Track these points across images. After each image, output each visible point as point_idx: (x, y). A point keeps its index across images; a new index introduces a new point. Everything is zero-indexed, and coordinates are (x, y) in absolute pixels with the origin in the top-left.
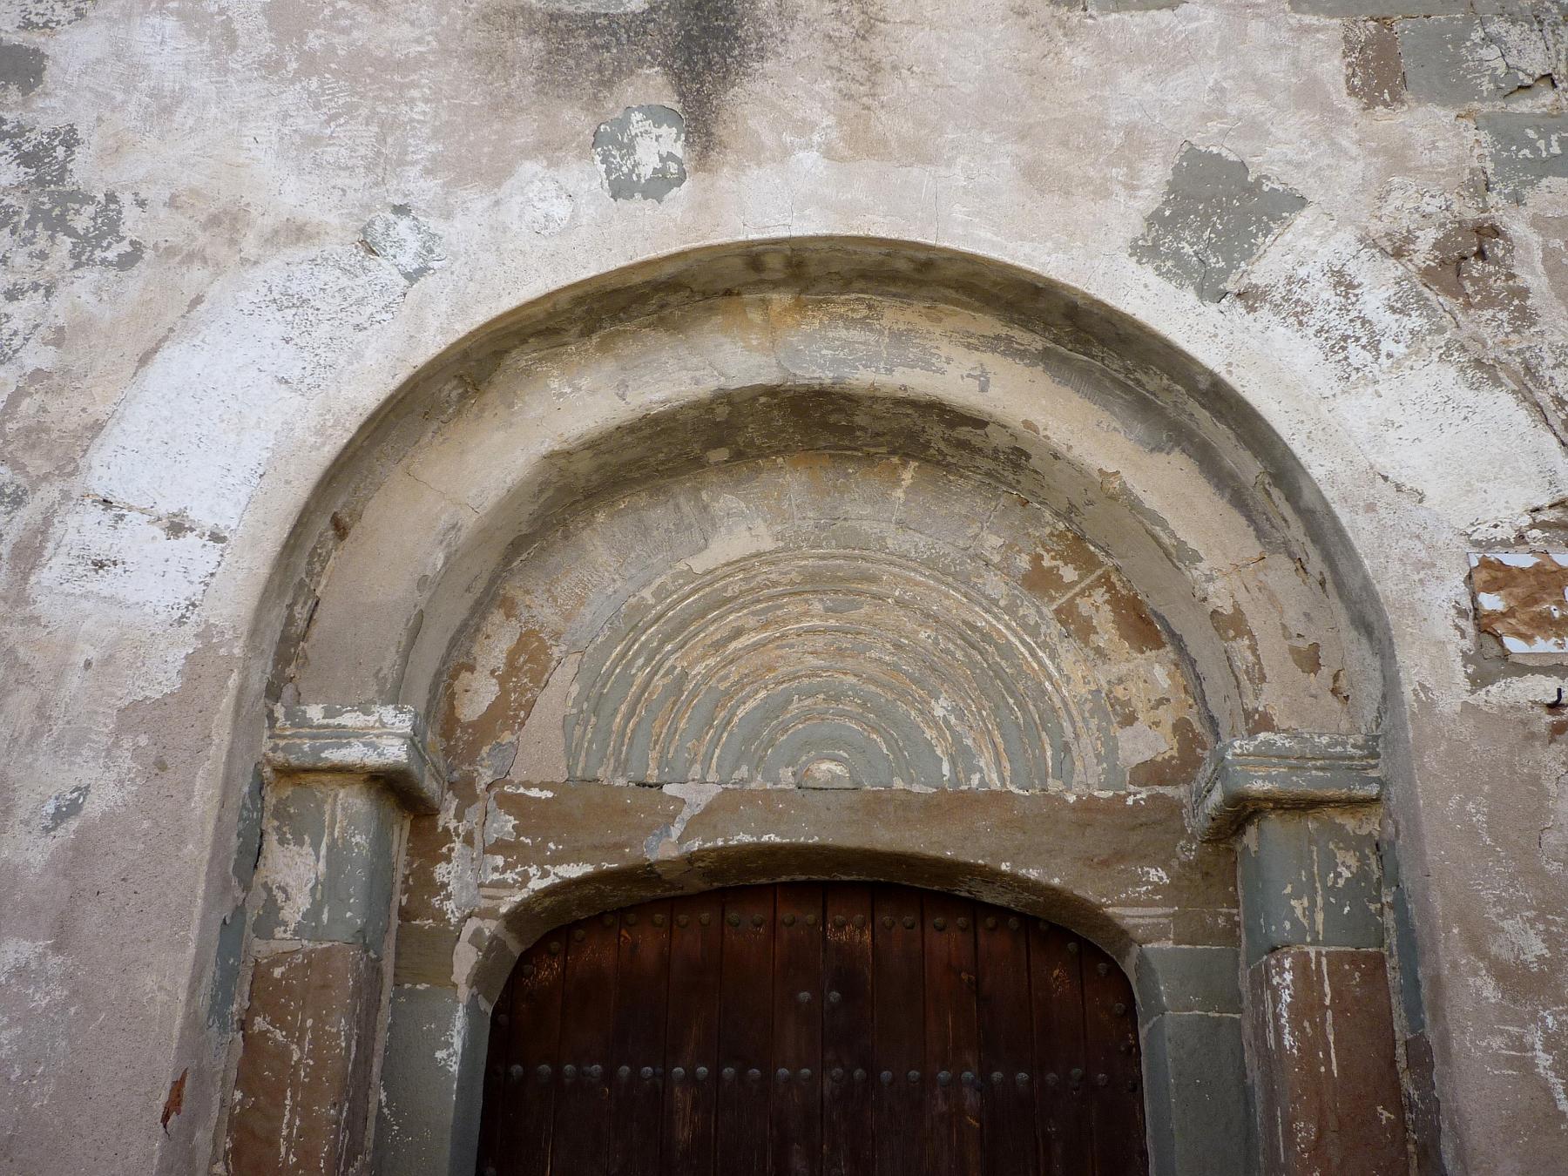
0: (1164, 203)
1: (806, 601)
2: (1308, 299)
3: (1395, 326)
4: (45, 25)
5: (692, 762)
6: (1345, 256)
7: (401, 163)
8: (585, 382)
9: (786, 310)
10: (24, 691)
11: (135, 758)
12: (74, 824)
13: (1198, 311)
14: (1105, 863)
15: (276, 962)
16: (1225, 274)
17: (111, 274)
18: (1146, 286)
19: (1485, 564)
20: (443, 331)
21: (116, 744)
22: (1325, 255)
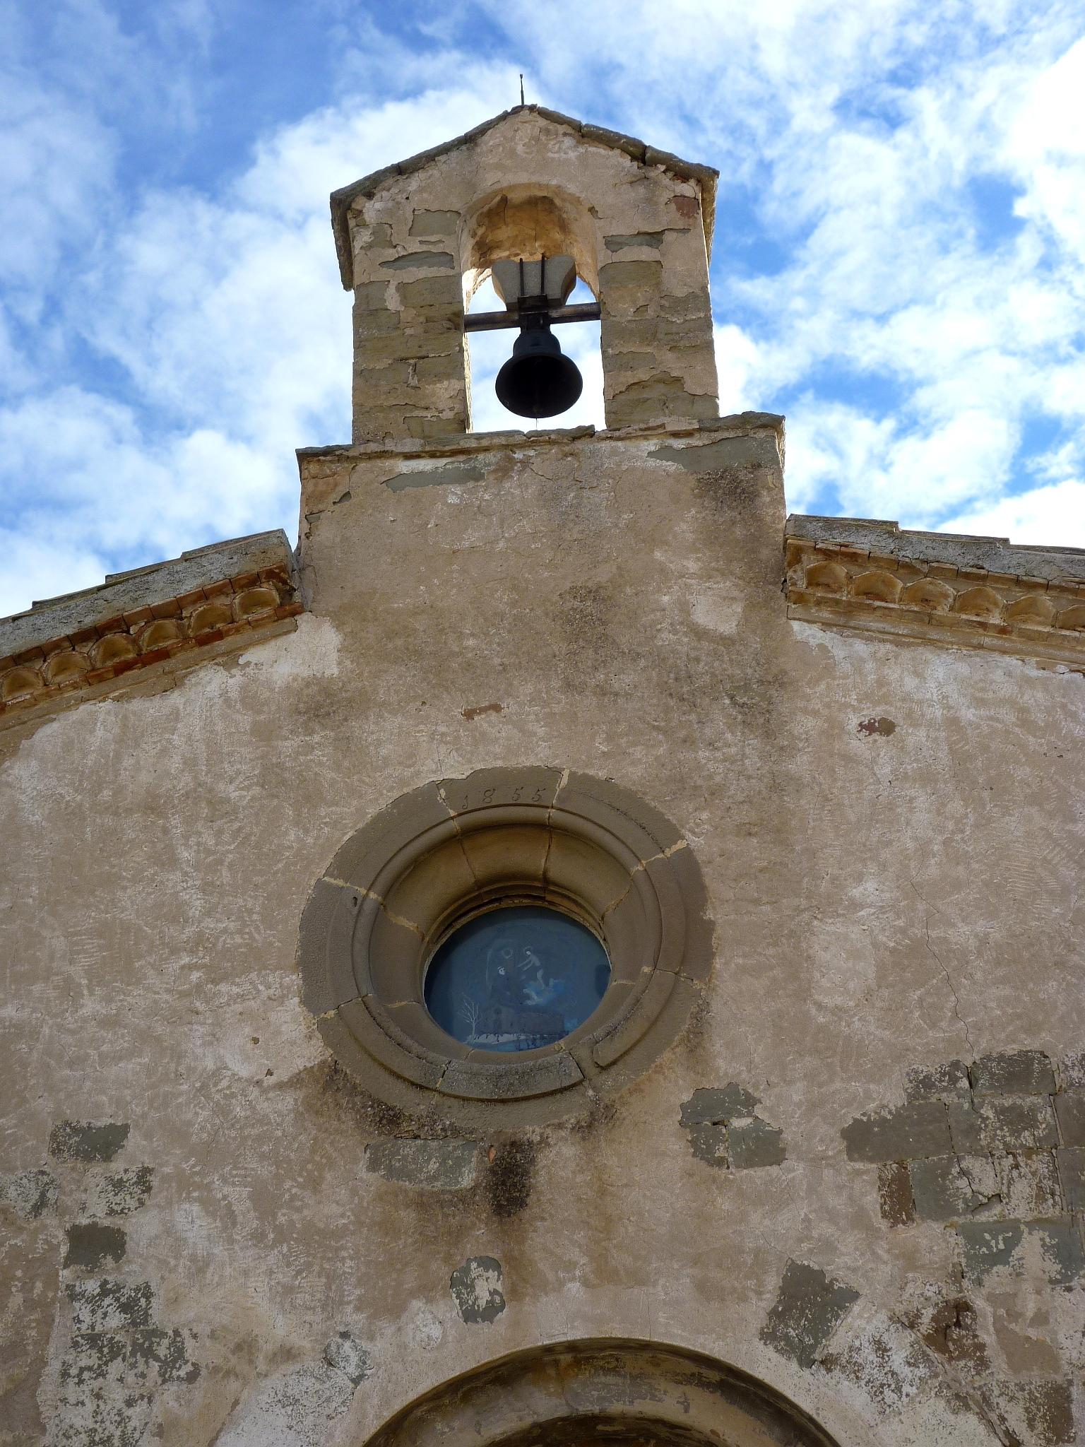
0: (778, 1302)
3: (910, 1375)
4: (122, 1212)
6: (882, 1330)
7: (342, 1303)
8: (456, 1424)
13: (799, 1374)
16: (814, 1347)
17: (184, 1386)
18: (769, 1360)
20: (378, 1417)
22: (870, 1330)
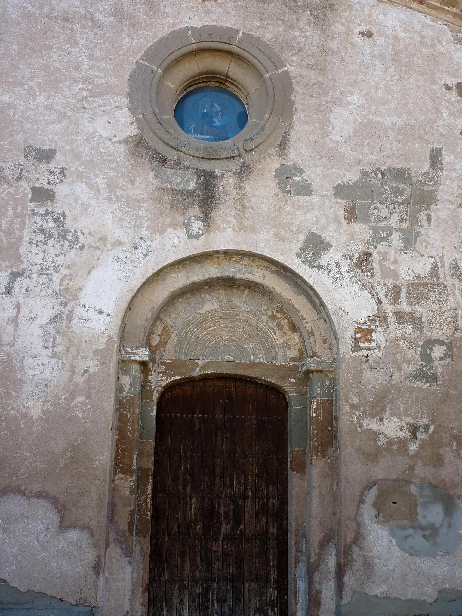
1: (224, 320)
2: (330, 269)
4: (54, 184)
5: (201, 355)
7: (141, 227)
8: (180, 275)
9: (223, 259)
10: (74, 347)
11: (98, 361)
12: (87, 374)
14: (283, 378)
15: (124, 398)
16: (315, 262)
17: (79, 251)
19: (358, 327)
20: (153, 269)
21: (94, 358)
